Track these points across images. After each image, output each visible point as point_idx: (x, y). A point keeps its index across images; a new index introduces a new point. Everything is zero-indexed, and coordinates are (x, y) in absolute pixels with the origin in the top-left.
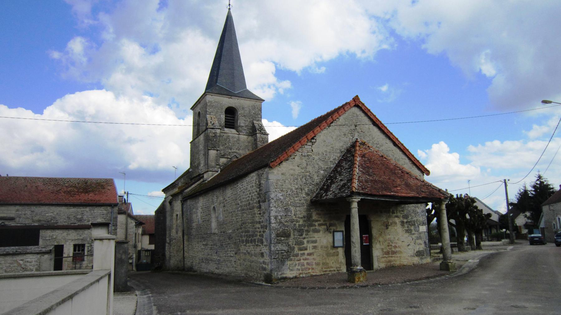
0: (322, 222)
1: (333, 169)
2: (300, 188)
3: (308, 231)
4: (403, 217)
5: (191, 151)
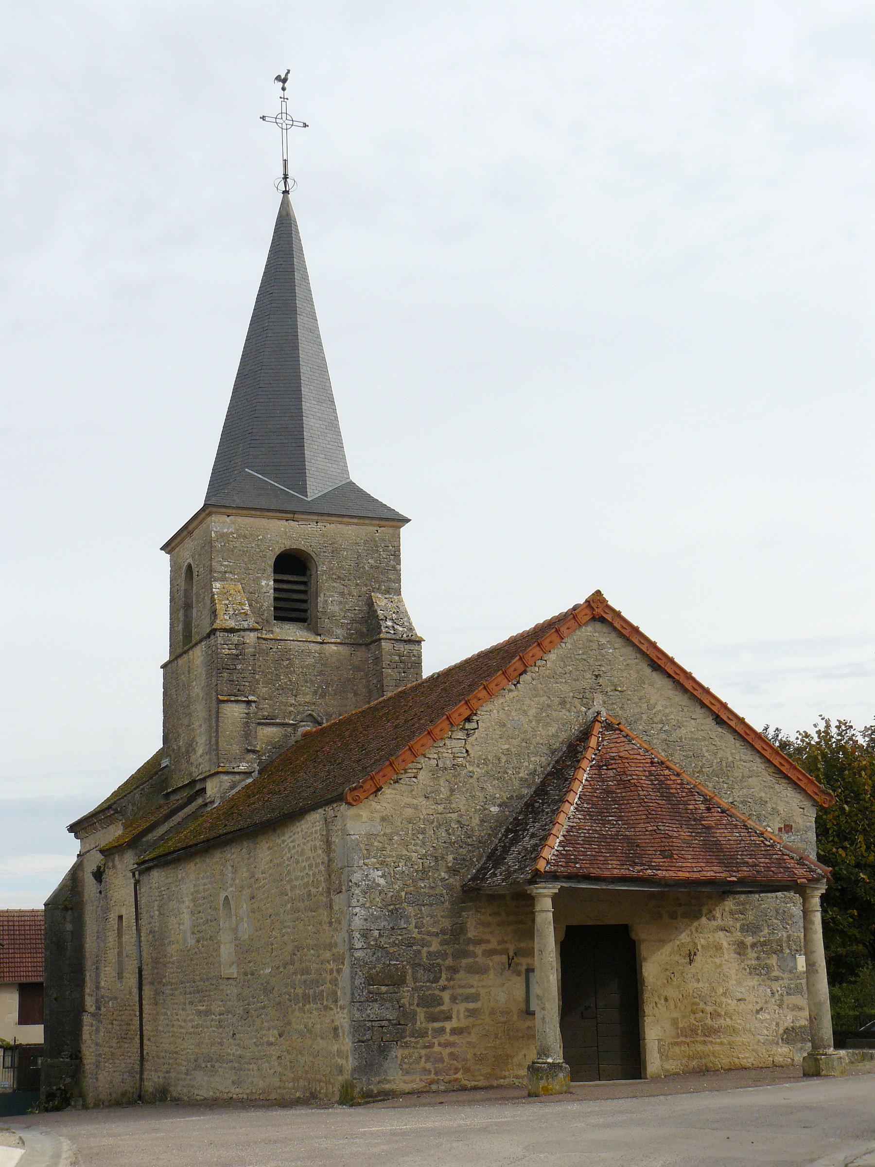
0: (493, 944)
1: (526, 800)
2: (431, 855)
3: (454, 970)
4: (742, 930)
5: (165, 694)
